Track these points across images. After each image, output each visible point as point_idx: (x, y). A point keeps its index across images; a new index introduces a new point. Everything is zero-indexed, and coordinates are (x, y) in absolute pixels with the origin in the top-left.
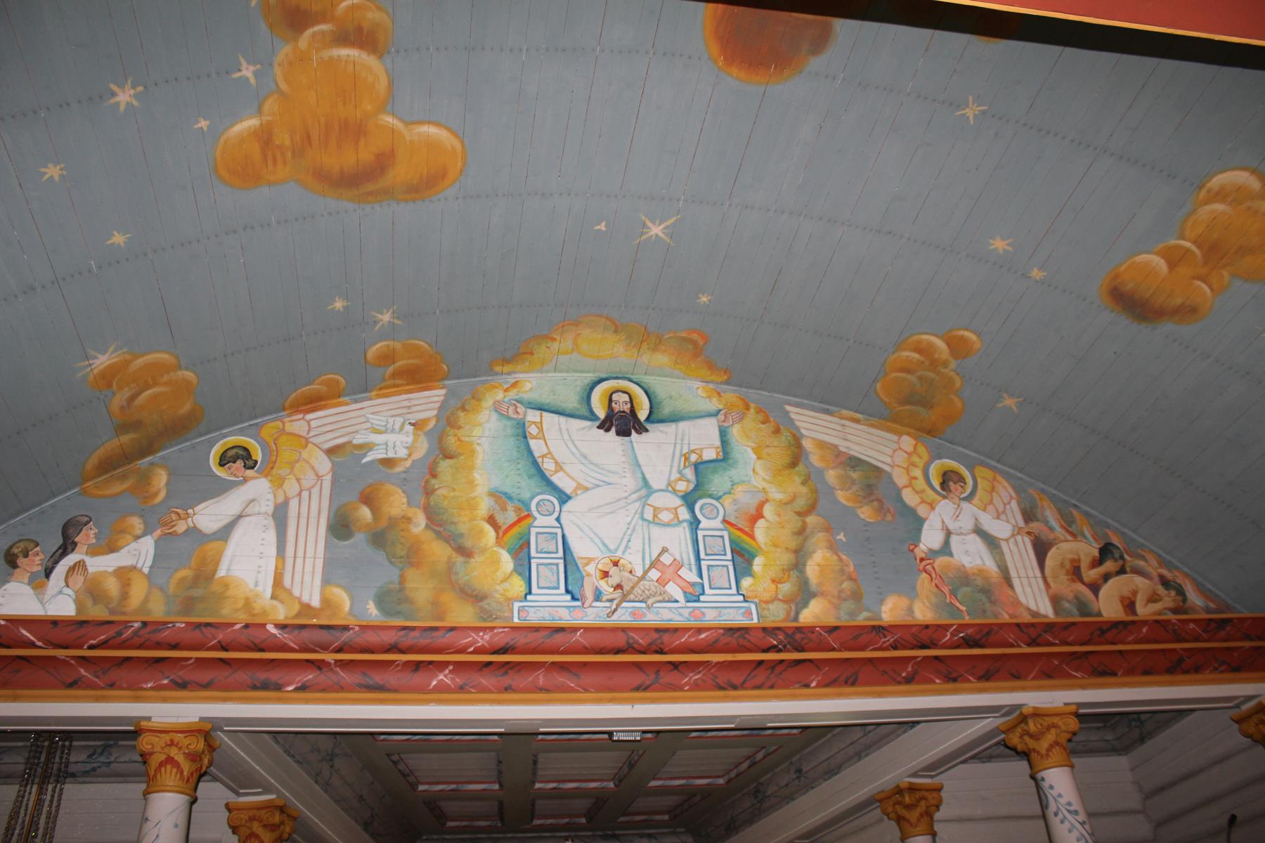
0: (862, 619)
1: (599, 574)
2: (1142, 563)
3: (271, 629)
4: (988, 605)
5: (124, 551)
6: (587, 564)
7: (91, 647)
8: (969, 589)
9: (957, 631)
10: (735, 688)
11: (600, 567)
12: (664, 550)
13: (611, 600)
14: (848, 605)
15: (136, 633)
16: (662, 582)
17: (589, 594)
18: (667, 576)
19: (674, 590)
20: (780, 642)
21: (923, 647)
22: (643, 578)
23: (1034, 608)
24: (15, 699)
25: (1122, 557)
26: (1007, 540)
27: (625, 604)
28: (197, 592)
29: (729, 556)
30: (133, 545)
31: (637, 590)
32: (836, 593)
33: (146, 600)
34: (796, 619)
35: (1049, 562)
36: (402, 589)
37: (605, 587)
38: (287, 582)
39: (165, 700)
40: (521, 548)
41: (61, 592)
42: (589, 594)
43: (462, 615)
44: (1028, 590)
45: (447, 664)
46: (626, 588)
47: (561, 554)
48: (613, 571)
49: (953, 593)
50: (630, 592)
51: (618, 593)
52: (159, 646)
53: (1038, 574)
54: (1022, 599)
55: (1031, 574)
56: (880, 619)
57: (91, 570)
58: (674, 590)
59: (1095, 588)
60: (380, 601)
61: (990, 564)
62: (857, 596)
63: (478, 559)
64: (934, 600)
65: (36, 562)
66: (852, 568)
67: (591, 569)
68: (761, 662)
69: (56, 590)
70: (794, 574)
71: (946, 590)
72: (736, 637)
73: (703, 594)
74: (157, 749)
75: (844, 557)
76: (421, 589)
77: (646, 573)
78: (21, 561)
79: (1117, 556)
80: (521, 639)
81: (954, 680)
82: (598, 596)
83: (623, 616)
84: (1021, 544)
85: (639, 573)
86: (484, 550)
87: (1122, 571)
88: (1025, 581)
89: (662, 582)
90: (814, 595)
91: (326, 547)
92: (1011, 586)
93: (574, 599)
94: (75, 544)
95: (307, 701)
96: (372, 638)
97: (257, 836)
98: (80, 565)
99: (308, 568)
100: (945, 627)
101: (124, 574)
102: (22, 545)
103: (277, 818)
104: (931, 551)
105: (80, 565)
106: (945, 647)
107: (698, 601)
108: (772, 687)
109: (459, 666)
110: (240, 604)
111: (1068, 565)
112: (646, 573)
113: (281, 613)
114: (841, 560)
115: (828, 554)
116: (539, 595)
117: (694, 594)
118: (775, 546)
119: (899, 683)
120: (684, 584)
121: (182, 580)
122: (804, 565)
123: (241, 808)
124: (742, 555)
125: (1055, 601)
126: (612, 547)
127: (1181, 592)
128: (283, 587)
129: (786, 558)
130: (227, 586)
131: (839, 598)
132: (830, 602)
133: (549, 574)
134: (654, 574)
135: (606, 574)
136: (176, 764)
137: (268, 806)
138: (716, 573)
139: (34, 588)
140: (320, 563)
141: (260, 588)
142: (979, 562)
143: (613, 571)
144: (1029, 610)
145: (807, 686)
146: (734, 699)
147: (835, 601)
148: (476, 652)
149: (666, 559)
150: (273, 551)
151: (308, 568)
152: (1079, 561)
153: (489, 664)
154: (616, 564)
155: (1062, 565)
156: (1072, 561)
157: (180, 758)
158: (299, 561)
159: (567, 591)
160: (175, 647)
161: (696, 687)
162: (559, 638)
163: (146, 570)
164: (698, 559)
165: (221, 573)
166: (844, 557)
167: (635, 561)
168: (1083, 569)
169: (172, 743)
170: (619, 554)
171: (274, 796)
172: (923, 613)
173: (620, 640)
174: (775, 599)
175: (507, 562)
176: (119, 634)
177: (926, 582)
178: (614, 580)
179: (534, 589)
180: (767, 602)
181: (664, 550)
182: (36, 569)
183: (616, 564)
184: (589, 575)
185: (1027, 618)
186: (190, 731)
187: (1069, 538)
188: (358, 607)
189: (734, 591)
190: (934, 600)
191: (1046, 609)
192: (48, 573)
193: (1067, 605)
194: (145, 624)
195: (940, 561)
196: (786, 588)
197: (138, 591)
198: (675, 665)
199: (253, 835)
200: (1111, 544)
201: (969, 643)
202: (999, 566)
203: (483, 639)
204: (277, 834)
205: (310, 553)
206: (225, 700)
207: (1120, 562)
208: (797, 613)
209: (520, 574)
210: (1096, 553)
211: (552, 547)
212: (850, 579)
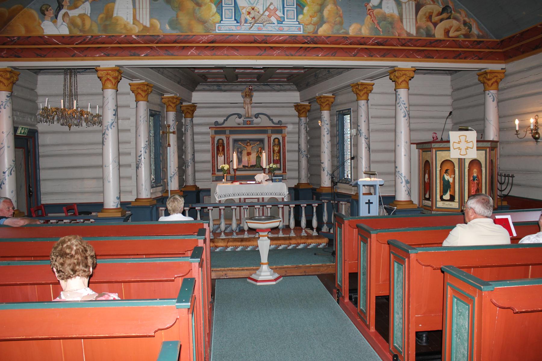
0: (341, 33)
1: (247, 13)
2: (458, 15)
3: (134, 37)
4: (391, 29)
5: (80, 8)
6: (243, 9)
7: (77, 44)
8: (385, 22)
9: (375, 40)
10: (292, 56)
11: (247, 10)
12: (271, 4)
13: (251, 23)
14: (337, 27)
15: (90, 39)
16: (269, 16)
17: (243, 21)
18: (271, 14)
19: (273, 19)
20: (309, 41)
21: (361, 44)
22: (263, 14)
23: (408, 31)
24: (57, 60)
25: (451, 12)
26: (405, 3)
27: (255, 25)
28: (108, 23)
29: (295, 6)
30: (83, 6)
31: (260, 19)
32: (333, 22)
33: (91, 26)
34: (316, 32)
35: (420, 13)
36: (177, 20)
37: (249, 18)
38: (138, 18)
39: (103, 60)
40: (219, 3)
41: (62, 24)
42: (243, 21)
43: (198, 30)
44: (408, 24)
45: (193, 47)
46: (256, 18)
47: (233, 5)
48: (252, 12)
49: (378, 24)
50: (257, 20)
51: (253, 20)
52: (98, 43)
53: (414, 17)
54: (405, 27)
55: (411, 17)
56: (348, 33)
57: (70, 15)
58: (273, 19)
59: (435, 24)
60: (171, 24)
61: (396, 13)
62: (341, 23)
63: (204, 8)
64: (370, 26)
65: (51, 13)
66: (341, 12)
67: (244, 11)
68: (301, 47)
69: (60, 23)
70: (319, 14)
71: (376, 22)
72: (294, 39)
73: (284, 21)
74: (104, 76)
75: (339, 8)
76: (184, 19)
77: (264, 12)
78: (46, 13)
79: (449, 11)
80: (218, 38)
81: (372, 56)
82: (246, 22)
83: (254, 31)
84: (411, 5)
85: (261, 13)
86: (206, 4)
87: (449, 18)
88: (408, 20)
89: (269, 16)
90: (325, 23)
91: (150, 4)
92: (402, 22)
93: (237, 22)
94: (63, 6)
95: (149, 59)
96: (167, 39)
97: (140, 94)
98: (66, 14)
99: (144, 12)
100: (370, 38)
101: (82, 16)
102: (45, 6)
103: (146, 88)
104: (374, 6)
105: (66, 14)
106: (369, 45)
107: (282, 24)
108: (305, 56)
109: (198, 48)
110: (123, 27)
111: (427, 15)
112: (264, 12)
113: (136, 30)
114: (337, 9)
115: (333, 7)
116: (225, 22)
117: (281, 21)
118: (313, 2)
119: (351, 56)
120: (277, 17)
121: (102, 18)
122: (323, 10)
123: (134, 85)
124: (300, 6)
125: (418, 29)
126: (252, 2)
127: (470, 28)
128: (136, 20)
129: (317, 8)
130: (117, 20)
131: (334, 24)
132: (331, 26)
133: (229, 13)
134: (267, 13)
135: (249, 13)
136: (110, 81)
137: (143, 84)
138: (289, 13)
139: (53, 23)
140: (148, 13)
141: (129, 20)
142: (392, 11)
143: (252, 12)
144: (406, 31)
145: (318, 56)
146: (292, 59)
147: (332, 25)
148: (203, 43)
149: (272, 7)
150: (131, 6)
151: (144, 12)
152: (433, 13)
153: (207, 47)
154: (253, 9)
155: (425, 14)
156: (430, 13)
157: (111, 78)
158: (141, 10)
159: (235, 20)
160: (103, 43)
161: (278, 55)
162: (231, 38)
163: (89, 15)
164: (284, 7)
165: (115, 15)
166: (339, 8)
167: (260, 8)
168: (433, 16)
169: (108, 74)
170: (254, 5)
171: (144, 81)
172: (365, 32)
173: (252, 39)
174: (311, 23)
175: (214, 8)
176: (85, 40)
177: (369, 19)
178: (252, 15)
179: (224, 19)
180: (307, 25)
181: (271, 4)
182: (53, 15)
183: (253, 9)
184: (243, 13)
185: (404, 36)
186: (113, 70)
187: (432, 3)
188: (163, 28)
189: (295, 20)
190: (370, 26)
191: (413, 32)
192: (56, 17)
193: (422, 30)
194: (92, 36)
195: (377, 11)
196: (315, 19)
197: (88, 23)
198: (271, 48)
199: (139, 93)
200: (448, 6)
201: (378, 44)
202: (399, 14)
203: (205, 39)
204: (146, 93)
205: (144, 7)
206: (122, 59)
207: (450, 14)
208: (318, 29)
209: (219, 13)
210: (441, 10)
211: (230, 3)
212: (340, 16)
